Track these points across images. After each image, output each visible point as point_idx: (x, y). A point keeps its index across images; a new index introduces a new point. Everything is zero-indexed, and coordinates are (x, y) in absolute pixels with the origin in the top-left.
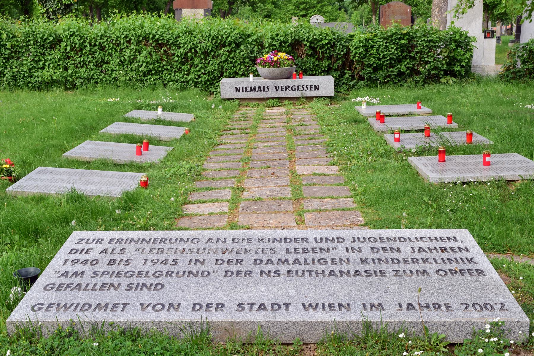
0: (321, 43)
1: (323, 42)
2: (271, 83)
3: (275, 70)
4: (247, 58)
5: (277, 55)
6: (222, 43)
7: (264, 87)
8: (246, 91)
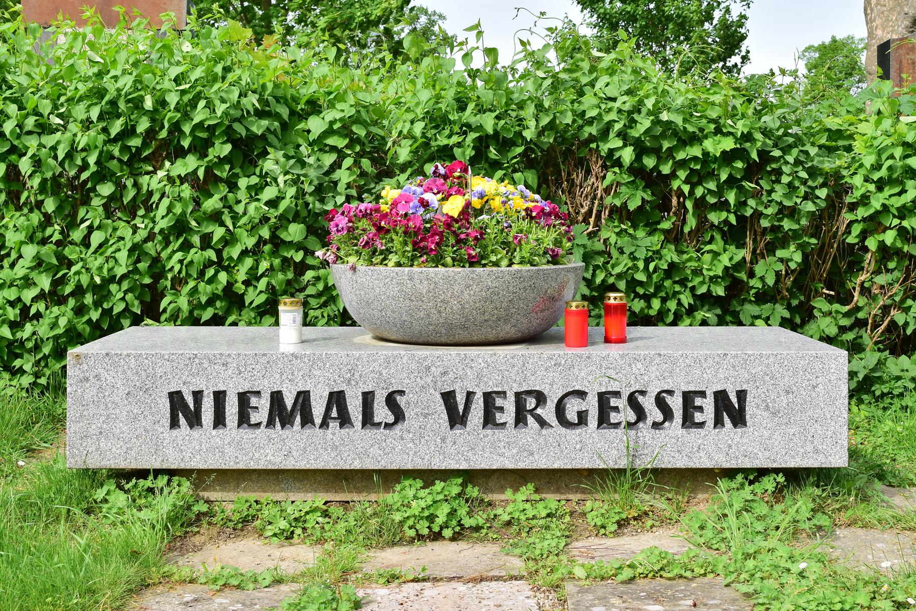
0: (695, 151)
1: (708, 144)
2: (423, 372)
3: (448, 285)
4: (296, 218)
5: (462, 187)
6: (163, 134)
7: (368, 399)
8: (243, 419)
